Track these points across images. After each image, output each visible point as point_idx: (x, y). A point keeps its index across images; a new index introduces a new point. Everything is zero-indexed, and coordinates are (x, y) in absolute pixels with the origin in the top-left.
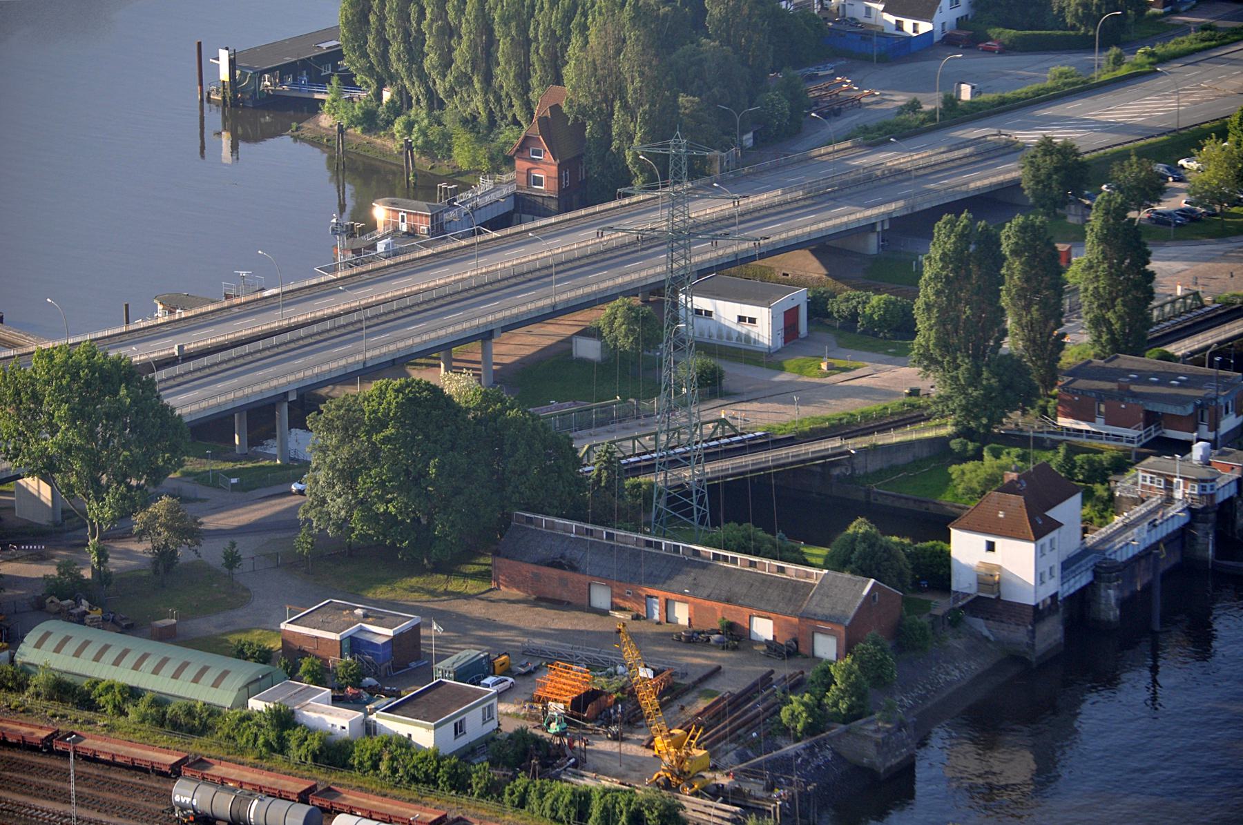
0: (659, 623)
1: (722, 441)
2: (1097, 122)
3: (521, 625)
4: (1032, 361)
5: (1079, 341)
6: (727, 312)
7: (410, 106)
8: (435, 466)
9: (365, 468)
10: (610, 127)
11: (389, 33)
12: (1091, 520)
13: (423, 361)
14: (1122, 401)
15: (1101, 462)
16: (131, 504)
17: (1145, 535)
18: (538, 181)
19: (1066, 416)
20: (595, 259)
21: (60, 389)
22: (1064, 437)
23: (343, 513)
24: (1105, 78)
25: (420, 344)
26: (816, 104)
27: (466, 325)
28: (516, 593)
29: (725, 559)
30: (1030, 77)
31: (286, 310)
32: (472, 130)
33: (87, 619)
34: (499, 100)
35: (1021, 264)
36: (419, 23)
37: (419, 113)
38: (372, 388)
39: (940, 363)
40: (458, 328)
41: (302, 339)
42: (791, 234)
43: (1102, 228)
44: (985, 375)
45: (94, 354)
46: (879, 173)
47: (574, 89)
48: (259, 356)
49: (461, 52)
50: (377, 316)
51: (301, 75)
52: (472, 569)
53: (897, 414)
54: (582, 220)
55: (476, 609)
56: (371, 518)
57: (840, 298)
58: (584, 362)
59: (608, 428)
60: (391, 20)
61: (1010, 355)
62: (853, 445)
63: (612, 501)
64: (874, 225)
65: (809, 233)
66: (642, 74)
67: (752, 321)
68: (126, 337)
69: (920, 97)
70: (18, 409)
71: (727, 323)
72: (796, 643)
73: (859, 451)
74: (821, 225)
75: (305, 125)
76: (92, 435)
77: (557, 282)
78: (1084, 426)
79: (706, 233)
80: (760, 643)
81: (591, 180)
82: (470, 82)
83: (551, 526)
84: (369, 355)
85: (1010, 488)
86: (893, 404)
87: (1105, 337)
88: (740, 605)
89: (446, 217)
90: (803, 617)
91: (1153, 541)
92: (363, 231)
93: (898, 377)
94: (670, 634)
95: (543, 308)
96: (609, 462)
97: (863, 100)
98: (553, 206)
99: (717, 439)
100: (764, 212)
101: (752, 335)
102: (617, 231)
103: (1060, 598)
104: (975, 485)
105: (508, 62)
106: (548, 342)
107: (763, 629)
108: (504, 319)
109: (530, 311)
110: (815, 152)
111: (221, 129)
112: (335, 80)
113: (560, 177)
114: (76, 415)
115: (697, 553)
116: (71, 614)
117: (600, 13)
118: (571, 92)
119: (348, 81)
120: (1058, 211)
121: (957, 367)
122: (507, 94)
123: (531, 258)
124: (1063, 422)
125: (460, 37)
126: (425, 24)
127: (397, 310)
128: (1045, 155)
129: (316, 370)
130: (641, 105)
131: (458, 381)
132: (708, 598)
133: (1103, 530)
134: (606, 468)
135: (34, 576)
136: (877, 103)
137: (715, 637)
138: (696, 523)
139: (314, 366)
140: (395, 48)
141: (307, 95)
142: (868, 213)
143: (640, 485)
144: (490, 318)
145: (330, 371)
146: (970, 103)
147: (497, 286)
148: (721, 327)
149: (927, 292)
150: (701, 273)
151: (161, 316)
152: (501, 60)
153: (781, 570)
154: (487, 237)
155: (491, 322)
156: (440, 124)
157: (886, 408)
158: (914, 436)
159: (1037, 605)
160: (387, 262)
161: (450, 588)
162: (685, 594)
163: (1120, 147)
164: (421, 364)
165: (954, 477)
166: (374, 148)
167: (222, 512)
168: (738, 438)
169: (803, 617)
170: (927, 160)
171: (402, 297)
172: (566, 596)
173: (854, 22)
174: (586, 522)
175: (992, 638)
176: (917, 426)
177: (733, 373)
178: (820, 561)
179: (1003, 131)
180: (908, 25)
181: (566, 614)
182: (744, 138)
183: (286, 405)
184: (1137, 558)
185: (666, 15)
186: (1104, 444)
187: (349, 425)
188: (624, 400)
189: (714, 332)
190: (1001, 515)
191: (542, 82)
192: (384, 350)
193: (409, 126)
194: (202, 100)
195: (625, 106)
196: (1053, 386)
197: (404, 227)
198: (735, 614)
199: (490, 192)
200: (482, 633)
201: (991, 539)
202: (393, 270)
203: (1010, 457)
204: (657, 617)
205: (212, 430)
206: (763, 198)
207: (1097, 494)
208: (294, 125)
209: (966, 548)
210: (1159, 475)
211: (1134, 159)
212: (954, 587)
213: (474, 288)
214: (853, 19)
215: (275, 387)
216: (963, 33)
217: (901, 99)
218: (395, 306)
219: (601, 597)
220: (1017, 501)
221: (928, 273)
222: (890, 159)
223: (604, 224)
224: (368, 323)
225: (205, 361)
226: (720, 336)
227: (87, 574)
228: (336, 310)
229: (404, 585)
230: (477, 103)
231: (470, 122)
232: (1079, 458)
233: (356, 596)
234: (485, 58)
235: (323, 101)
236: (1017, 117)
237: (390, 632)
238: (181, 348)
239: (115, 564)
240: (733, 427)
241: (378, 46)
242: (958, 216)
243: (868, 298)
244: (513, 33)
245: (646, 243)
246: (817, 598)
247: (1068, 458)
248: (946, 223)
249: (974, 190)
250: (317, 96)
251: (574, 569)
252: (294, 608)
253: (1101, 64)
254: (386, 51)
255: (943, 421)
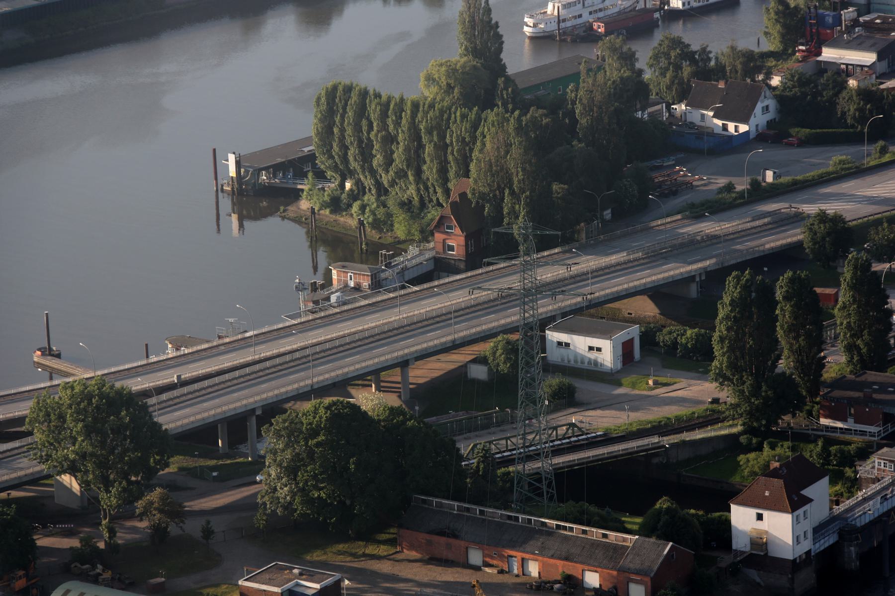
0: (517, 576)
1: (573, 439)
2: (865, 197)
3: (417, 578)
4: (800, 377)
5: (836, 361)
6: (581, 343)
7: (364, 193)
8: (354, 463)
9: (304, 465)
10: (502, 208)
11: (348, 140)
12: (842, 495)
13: (360, 382)
14: (867, 406)
15: (849, 451)
16: (130, 496)
17: (879, 506)
18: (451, 248)
19: (826, 417)
20: (486, 306)
21: (78, 412)
22: (824, 433)
23: (288, 498)
24: (872, 163)
25: (354, 371)
26: (660, 187)
27: (388, 357)
28: (414, 555)
29: (565, 528)
30: (820, 164)
31: (258, 348)
32: (409, 210)
33: (101, 578)
34: (427, 188)
35: (791, 306)
36: (368, 133)
37: (370, 198)
38: (308, 406)
39: (731, 380)
40: (382, 359)
41: (268, 368)
42: (631, 285)
43: (852, 278)
44: (764, 388)
45: (104, 385)
46: (699, 238)
47: (476, 181)
48: (235, 382)
49: (399, 155)
50: (324, 351)
51: (289, 172)
52: (384, 537)
53: (702, 417)
54: (480, 277)
55: (385, 567)
56: (309, 501)
57: (665, 331)
58: (474, 381)
59: (489, 431)
60: (349, 131)
61: (784, 373)
62: (667, 441)
63: (491, 486)
64: (694, 277)
65: (645, 284)
66: (524, 169)
67: (599, 350)
68: (141, 369)
69: (734, 180)
70: (49, 426)
71: (581, 352)
72: (616, 590)
73: (673, 445)
74: (654, 278)
75: (289, 208)
76: (103, 445)
77: (456, 323)
78: (839, 425)
79: (549, 290)
80: (589, 590)
81: (488, 244)
82: (406, 176)
83: (440, 505)
84: (315, 380)
85: (775, 474)
86: (700, 409)
87: (856, 358)
88: (576, 562)
89: (383, 275)
90: (621, 570)
91: (885, 510)
92: (323, 287)
93: (699, 391)
94: (525, 584)
95: (445, 343)
96: (484, 456)
97: (694, 183)
98: (462, 266)
99: (552, 441)
100: (613, 269)
101: (599, 360)
102: (485, 290)
103: (813, 554)
104: (756, 469)
105: (432, 161)
106: (452, 367)
107: (592, 579)
108: (416, 351)
109: (436, 346)
110: (654, 224)
111: (231, 211)
112: (310, 175)
113: (467, 245)
114: (88, 431)
115: (544, 524)
116: (89, 576)
117: (493, 125)
118: (473, 184)
119: (320, 175)
120: (831, 264)
121: (744, 383)
122: (433, 185)
123: (440, 306)
124: (824, 421)
125: (398, 143)
126: (372, 135)
127: (339, 346)
128: (820, 223)
129: (276, 392)
130: (524, 192)
131: (372, 400)
132: (552, 557)
133: (847, 502)
134: (483, 462)
135: (65, 547)
136: (705, 185)
137: (557, 586)
138: (546, 501)
139: (274, 389)
140: (352, 152)
141: (293, 186)
142: (689, 268)
143: (509, 473)
144: (406, 351)
145: (287, 392)
146: (771, 185)
147: (413, 327)
148: (576, 354)
149: (721, 328)
150: (564, 315)
151: (171, 353)
152: (427, 159)
153: (605, 536)
154: (409, 290)
155: (406, 354)
156: (385, 206)
157: (694, 413)
158: (713, 434)
159: (795, 560)
160: (337, 310)
161: (367, 552)
162: (535, 554)
163: (880, 216)
164: (358, 385)
165: (741, 463)
166: (339, 224)
167: (204, 497)
168: (584, 437)
169: (621, 570)
170: (734, 228)
171: (344, 336)
172: (451, 556)
173: (692, 125)
174: (464, 502)
175: (762, 584)
176: (716, 427)
177: (584, 387)
178: (635, 527)
179: (793, 205)
180: (731, 126)
181: (450, 570)
182: (605, 213)
183: (254, 418)
184: (873, 523)
185: (547, 124)
186: (855, 438)
187: (293, 433)
188: (502, 409)
189: (572, 358)
190: (767, 494)
191: (457, 175)
192: (327, 376)
193: (363, 208)
194: (217, 190)
195: (512, 193)
196: (817, 394)
197: (352, 284)
198: (573, 569)
199: (417, 256)
200: (388, 585)
201: (760, 511)
202: (339, 316)
203: (784, 449)
204: (516, 571)
205: (199, 438)
206: (613, 259)
207: (847, 475)
208: (282, 208)
209: (742, 518)
210: (891, 461)
211: (886, 225)
212: (734, 547)
213: (397, 329)
214: (691, 123)
215: (246, 405)
216: (772, 132)
217: (722, 181)
218: (337, 343)
219: (475, 557)
220: (778, 483)
221: (721, 314)
222: (709, 227)
223: (475, 287)
224: (456, 314)
225: (196, 386)
226: (576, 361)
227: (101, 545)
228: (295, 347)
229: (334, 550)
230: (412, 191)
231: (406, 205)
232: (833, 449)
233: (296, 558)
234: (415, 160)
235: (302, 190)
236: (804, 195)
237: (317, 586)
238: (179, 377)
239: (122, 538)
240: (580, 429)
241: (340, 150)
242: (743, 272)
243: (685, 331)
244: (435, 139)
245: (504, 300)
246: (630, 557)
247: (825, 448)
248: (734, 278)
249: (769, 250)
250: (299, 187)
251: (456, 537)
252: (250, 569)
253: (870, 153)
254: (346, 154)
255: (736, 422)
